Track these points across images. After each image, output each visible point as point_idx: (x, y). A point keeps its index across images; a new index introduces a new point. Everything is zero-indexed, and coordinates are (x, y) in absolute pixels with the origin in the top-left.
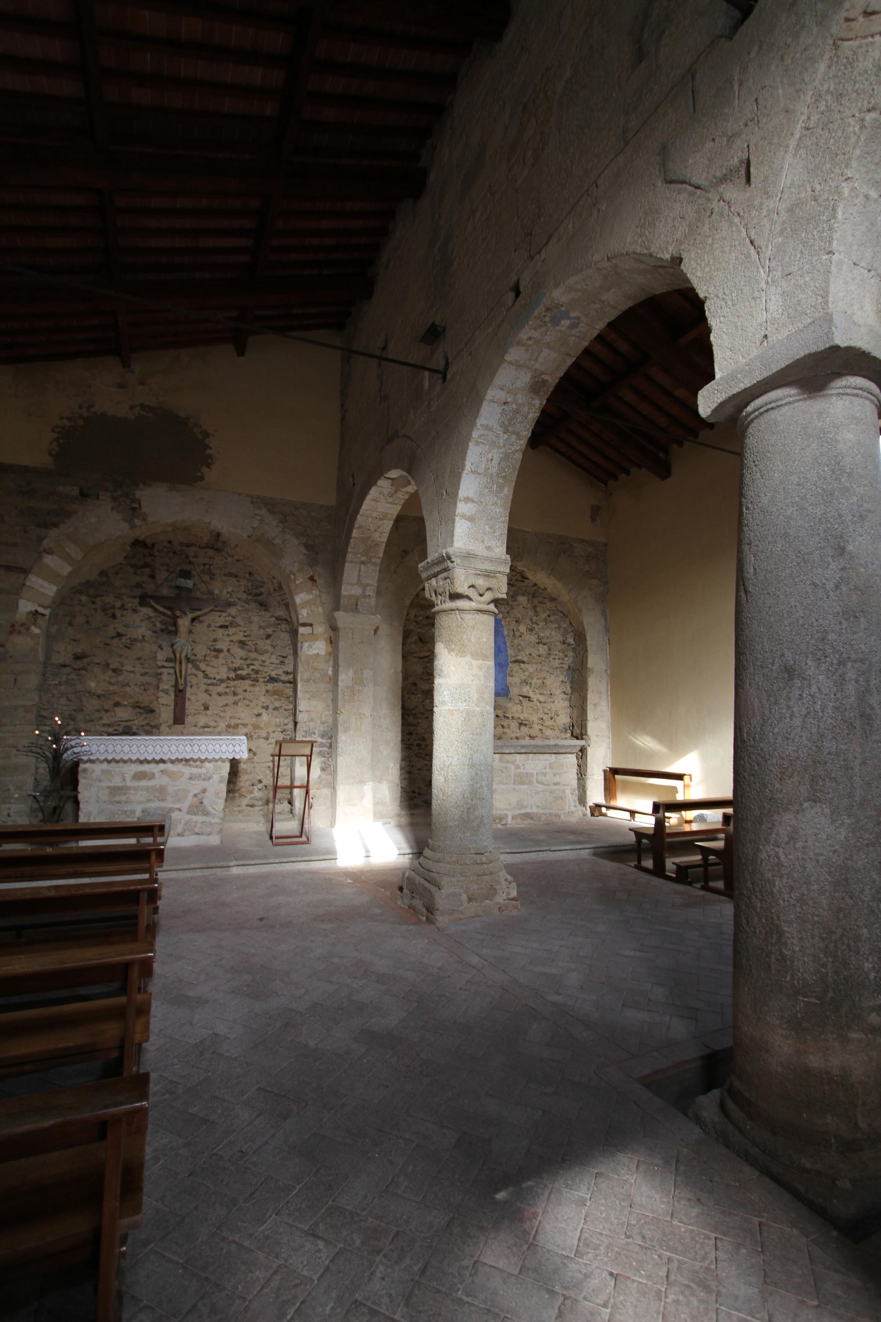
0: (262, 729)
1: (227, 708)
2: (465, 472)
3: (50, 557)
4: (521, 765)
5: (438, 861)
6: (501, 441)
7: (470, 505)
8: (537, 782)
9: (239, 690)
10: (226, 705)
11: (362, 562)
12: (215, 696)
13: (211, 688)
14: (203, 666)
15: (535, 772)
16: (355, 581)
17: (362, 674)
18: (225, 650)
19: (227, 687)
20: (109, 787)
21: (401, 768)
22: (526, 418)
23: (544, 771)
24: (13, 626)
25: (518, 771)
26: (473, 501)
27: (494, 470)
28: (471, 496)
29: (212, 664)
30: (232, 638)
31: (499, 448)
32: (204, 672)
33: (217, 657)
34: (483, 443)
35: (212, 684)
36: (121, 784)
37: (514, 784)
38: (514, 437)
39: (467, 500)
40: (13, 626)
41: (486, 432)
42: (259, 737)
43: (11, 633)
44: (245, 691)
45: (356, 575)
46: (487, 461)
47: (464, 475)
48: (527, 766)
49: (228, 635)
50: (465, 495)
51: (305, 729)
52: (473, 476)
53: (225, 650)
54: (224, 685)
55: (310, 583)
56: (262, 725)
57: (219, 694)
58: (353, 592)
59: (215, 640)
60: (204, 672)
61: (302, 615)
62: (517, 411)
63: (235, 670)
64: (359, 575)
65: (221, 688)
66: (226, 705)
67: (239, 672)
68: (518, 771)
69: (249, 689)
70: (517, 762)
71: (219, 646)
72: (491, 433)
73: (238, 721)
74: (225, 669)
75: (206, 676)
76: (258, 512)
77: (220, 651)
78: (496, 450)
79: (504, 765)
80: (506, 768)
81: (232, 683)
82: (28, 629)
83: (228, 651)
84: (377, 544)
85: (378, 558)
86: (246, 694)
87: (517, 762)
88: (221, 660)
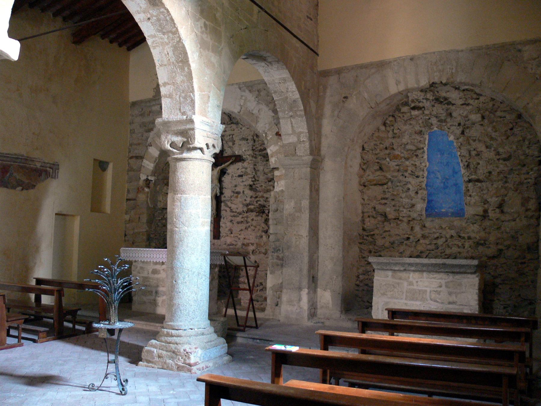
0: (262, 246)
1: (242, 232)
2: (157, 67)
3: (150, 147)
4: (414, 282)
5: (180, 336)
6: (166, 40)
7: (168, 87)
8: (431, 300)
9: (249, 220)
10: (242, 230)
11: (291, 116)
12: (235, 224)
13: (233, 218)
14: (229, 204)
15: (428, 290)
16: (291, 132)
17: (301, 204)
18: (241, 192)
19: (242, 218)
20: (143, 277)
21: (53, 265)
22: (167, 20)
23: (439, 289)
24: (138, 189)
25: (412, 287)
26: (169, 84)
27: (173, 60)
28: (166, 81)
29: (234, 202)
30: (245, 183)
31: (167, 44)
32: (230, 208)
33: (237, 197)
34: (157, 46)
35: (234, 216)
36: (146, 276)
37: (406, 299)
38: (170, 35)
39: (165, 84)
40: (138, 189)
41: (154, 39)
42: (260, 253)
43: (138, 192)
44: (253, 220)
45: (290, 127)
46: (166, 55)
47: (157, 69)
48: (419, 283)
49: (243, 181)
50: (163, 82)
51: (274, 247)
52: (162, 68)
53: (241, 192)
54: (241, 216)
55: (276, 137)
56: (262, 244)
57: (238, 223)
58: (291, 141)
59: (236, 186)
60: (230, 208)
61: (272, 162)
62: (159, 20)
63: (247, 205)
64: (292, 126)
65: (239, 219)
66: (242, 230)
67: (250, 207)
68: (412, 287)
69: (255, 218)
70: (411, 279)
71: (238, 189)
72: (157, 39)
73: (248, 241)
74: (241, 206)
75: (232, 211)
76: (243, 94)
77: (238, 193)
78: (167, 47)
79: (397, 281)
80: (398, 284)
81: (245, 215)
82: (143, 189)
83: (243, 192)
84: (294, 101)
85: (301, 110)
86: (253, 222)
87: (411, 279)
88: (239, 199)
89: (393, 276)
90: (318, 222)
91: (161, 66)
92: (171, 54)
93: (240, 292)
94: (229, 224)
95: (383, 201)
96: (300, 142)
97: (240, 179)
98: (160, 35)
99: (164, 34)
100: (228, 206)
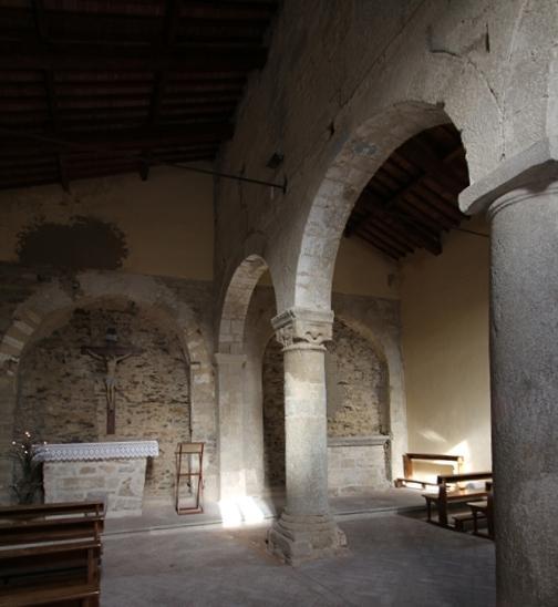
9: (151, 409)
14: (126, 394)
39: (303, 274)
57: (138, 413)
59: (134, 376)
62: (335, 212)
63: (148, 396)
65: (139, 409)
71: (136, 379)
75: (129, 401)
82: (5, 373)
89: (332, 451)
90: (281, 408)
91: (306, 254)
92: (322, 247)
93: (488, 469)
94: (126, 414)
95: (42, 395)
96: (235, 342)
97: (137, 370)
98: (324, 226)
99: (328, 226)
100: (122, 395)
